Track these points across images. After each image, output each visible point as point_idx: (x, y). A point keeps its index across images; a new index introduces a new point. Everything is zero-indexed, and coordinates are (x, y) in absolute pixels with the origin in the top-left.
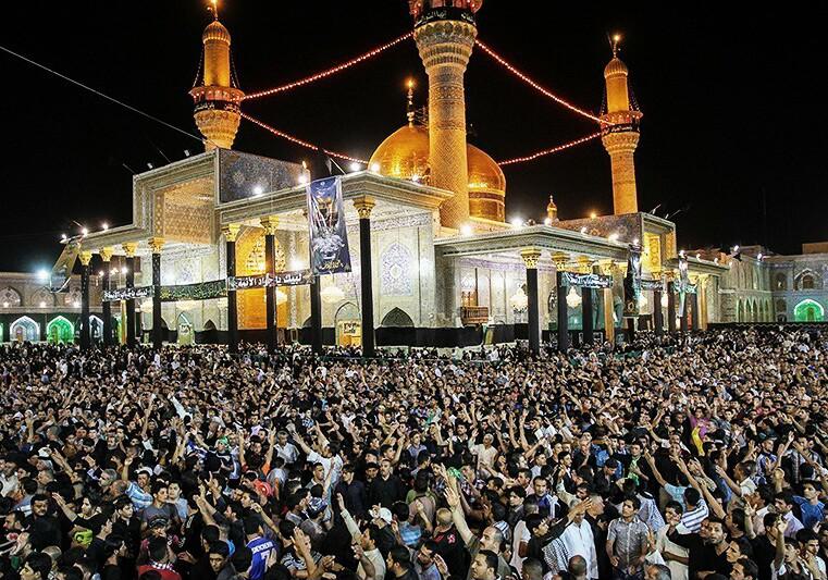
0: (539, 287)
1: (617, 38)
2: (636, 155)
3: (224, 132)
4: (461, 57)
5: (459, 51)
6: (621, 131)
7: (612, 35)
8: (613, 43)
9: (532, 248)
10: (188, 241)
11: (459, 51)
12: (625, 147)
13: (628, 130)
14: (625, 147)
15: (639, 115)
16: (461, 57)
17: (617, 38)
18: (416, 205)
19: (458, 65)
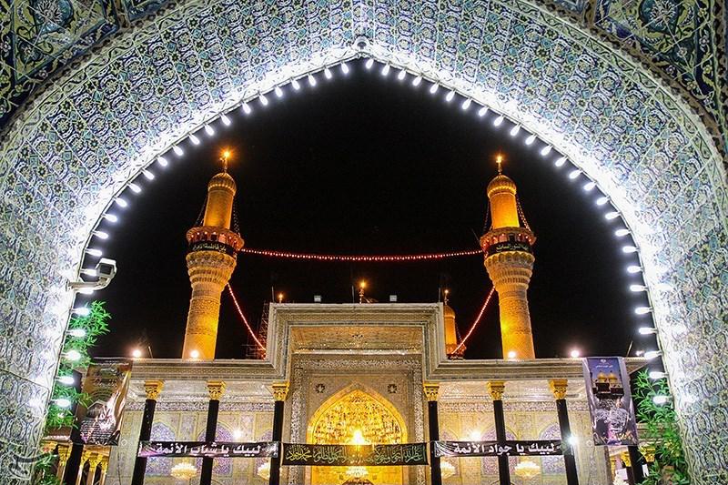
4: (525, 277)
16: (525, 277)
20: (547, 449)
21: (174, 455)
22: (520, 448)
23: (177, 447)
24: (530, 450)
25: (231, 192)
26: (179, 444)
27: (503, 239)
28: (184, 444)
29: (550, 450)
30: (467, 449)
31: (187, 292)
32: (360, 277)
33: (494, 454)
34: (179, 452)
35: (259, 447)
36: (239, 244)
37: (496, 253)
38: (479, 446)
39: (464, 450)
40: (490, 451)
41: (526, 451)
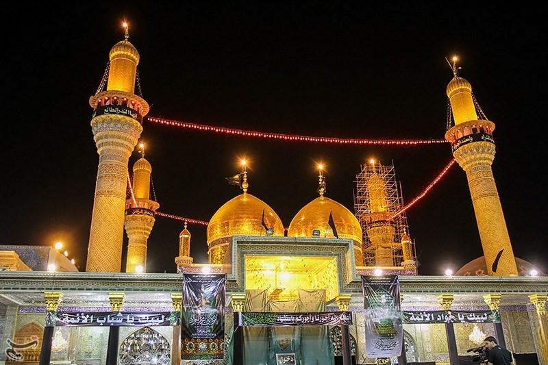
0: (454, 328)
1: (455, 59)
2: (495, 167)
3: (134, 228)
4: (129, 144)
5: (130, 141)
6: (461, 145)
7: (449, 54)
8: (452, 64)
9: (500, 294)
10: (116, 51)
11: (130, 141)
12: (481, 159)
13: (469, 142)
14: (481, 159)
15: (491, 127)
16: (129, 144)
17: (455, 59)
18: (512, 300)
19: (125, 150)
20: (482, 318)
21: (80, 324)
22: (461, 317)
23: (83, 317)
24: (469, 318)
25: (468, 91)
26: (427, 313)
27: (467, 132)
28: (90, 314)
29: (484, 318)
30: (76, 318)
31: (96, 158)
32: (318, 158)
33: (442, 321)
34: (428, 319)
35: (163, 317)
36: (144, 107)
37: (103, 114)
38: (429, 315)
39: (418, 318)
40: (438, 319)
41: (466, 319)
